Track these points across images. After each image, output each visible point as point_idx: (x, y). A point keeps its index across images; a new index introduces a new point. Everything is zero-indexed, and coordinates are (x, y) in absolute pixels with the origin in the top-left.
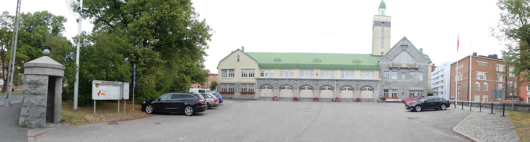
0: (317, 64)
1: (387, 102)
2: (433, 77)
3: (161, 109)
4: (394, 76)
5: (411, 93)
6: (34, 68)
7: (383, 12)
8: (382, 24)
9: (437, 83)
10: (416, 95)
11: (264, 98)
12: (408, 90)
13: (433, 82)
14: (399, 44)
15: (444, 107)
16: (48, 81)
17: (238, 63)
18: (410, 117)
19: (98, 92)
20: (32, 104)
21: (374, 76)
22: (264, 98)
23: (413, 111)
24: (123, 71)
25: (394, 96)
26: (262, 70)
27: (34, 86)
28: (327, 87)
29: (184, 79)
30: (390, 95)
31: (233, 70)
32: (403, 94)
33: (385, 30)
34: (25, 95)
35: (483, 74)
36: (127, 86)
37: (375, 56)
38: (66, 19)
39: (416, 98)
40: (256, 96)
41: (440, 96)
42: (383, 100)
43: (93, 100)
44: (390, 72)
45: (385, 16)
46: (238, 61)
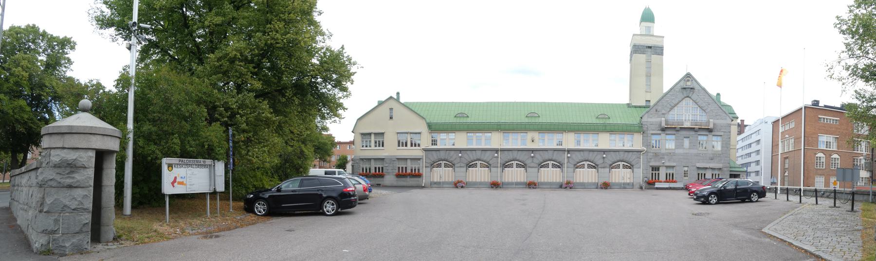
0: (533, 121)
1: (657, 189)
2: (741, 144)
3: (282, 207)
4: (669, 143)
5: (701, 172)
6: (67, 136)
8: (647, 51)
9: (749, 155)
10: (709, 176)
11: (439, 185)
13: (740, 152)
15: (755, 197)
16: (94, 160)
17: (391, 121)
18: (696, 212)
19: (172, 180)
20: (65, 206)
21: (634, 142)
22: (439, 185)
23: (704, 203)
24: (214, 139)
25: (670, 178)
26: (434, 135)
27: (68, 170)
28: (550, 163)
29: (302, 152)
30: (663, 177)
31: (383, 134)
32: (686, 174)
34: (48, 190)
35: (830, 138)
36: (220, 167)
37: (636, 107)
38: (75, 43)
39: (708, 182)
40: (424, 181)
41: (751, 179)
42: (650, 184)
43: (164, 195)
44: (663, 136)
45: (653, 36)
46: (391, 118)
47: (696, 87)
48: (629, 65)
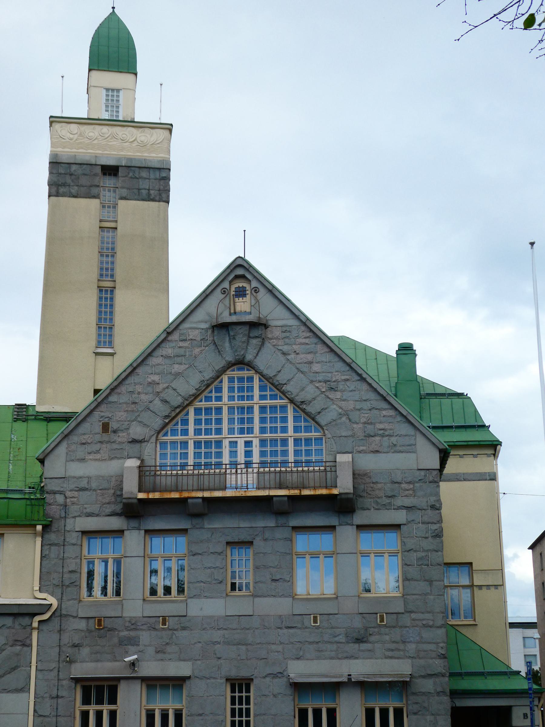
7: (113, 93)
8: (109, 183)
12: (279, 686)
33: (124, 227)
44: (134, 540)
45: (131, 123)
47: (277, 317)
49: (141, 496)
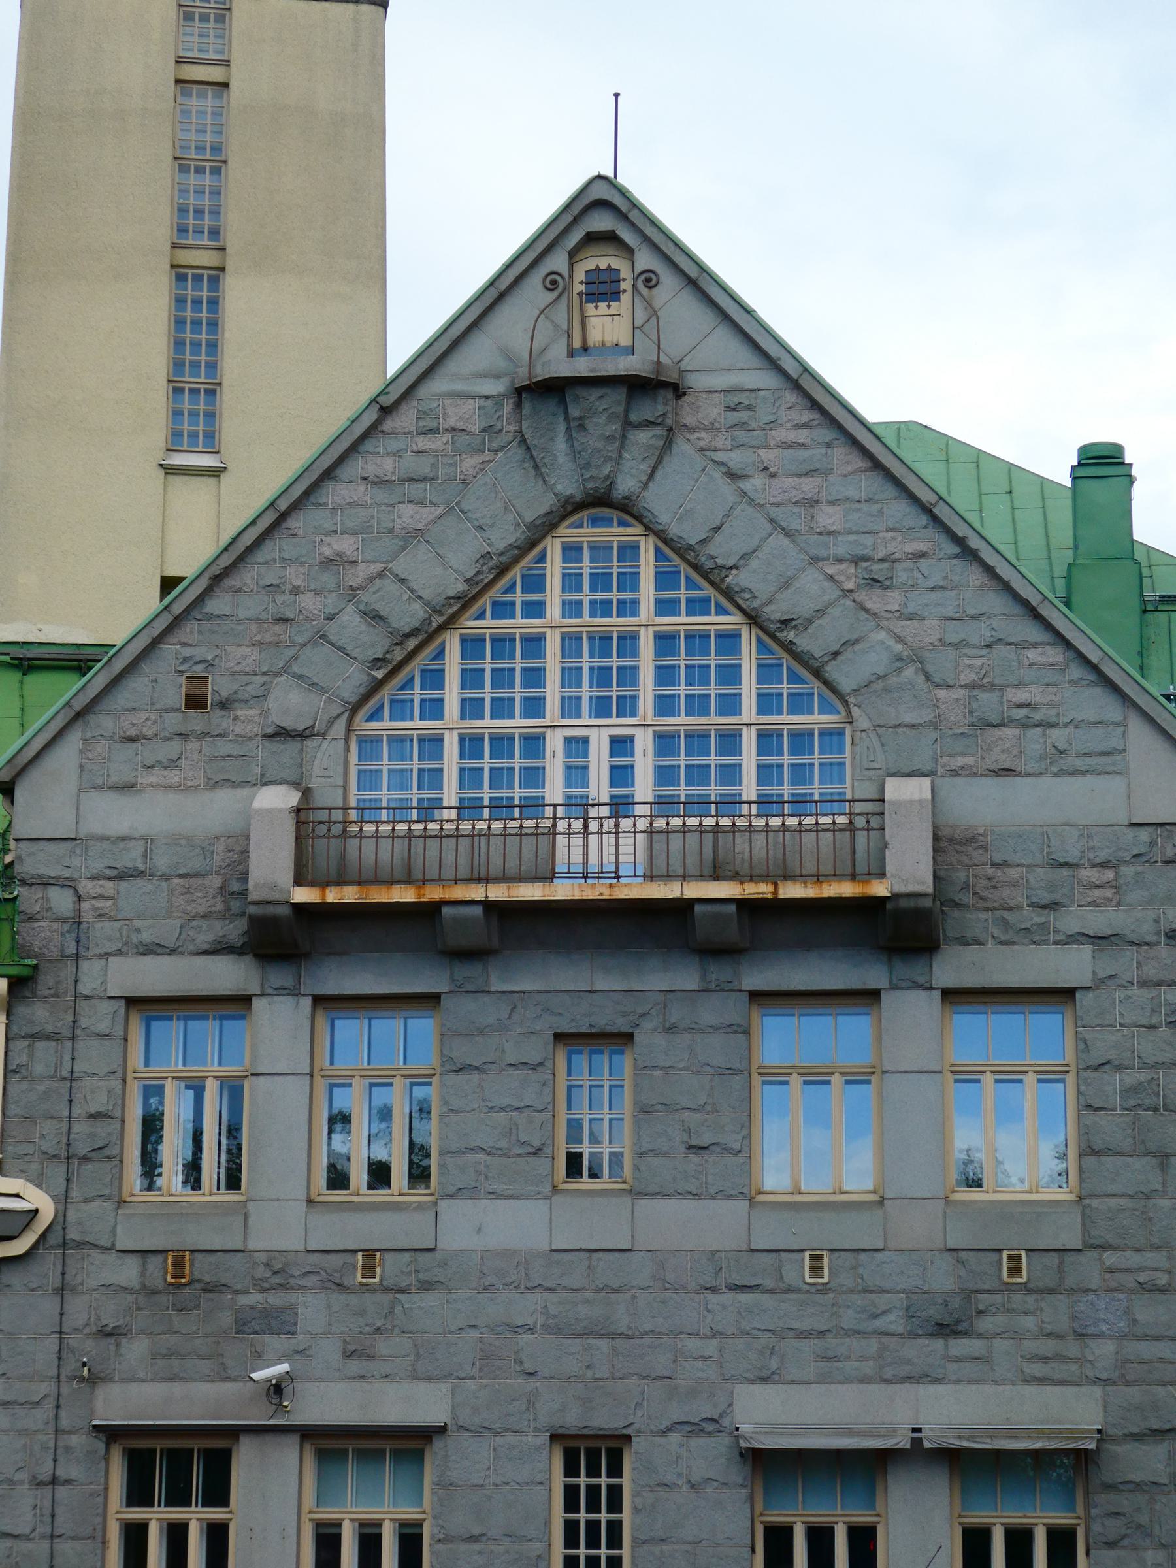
12: (708, 1457)
14: (483, 369)
44: (279, 1025)
46: (617, 95)
47: (711, 362)
48: (876, 395)
49: (303, 895)
